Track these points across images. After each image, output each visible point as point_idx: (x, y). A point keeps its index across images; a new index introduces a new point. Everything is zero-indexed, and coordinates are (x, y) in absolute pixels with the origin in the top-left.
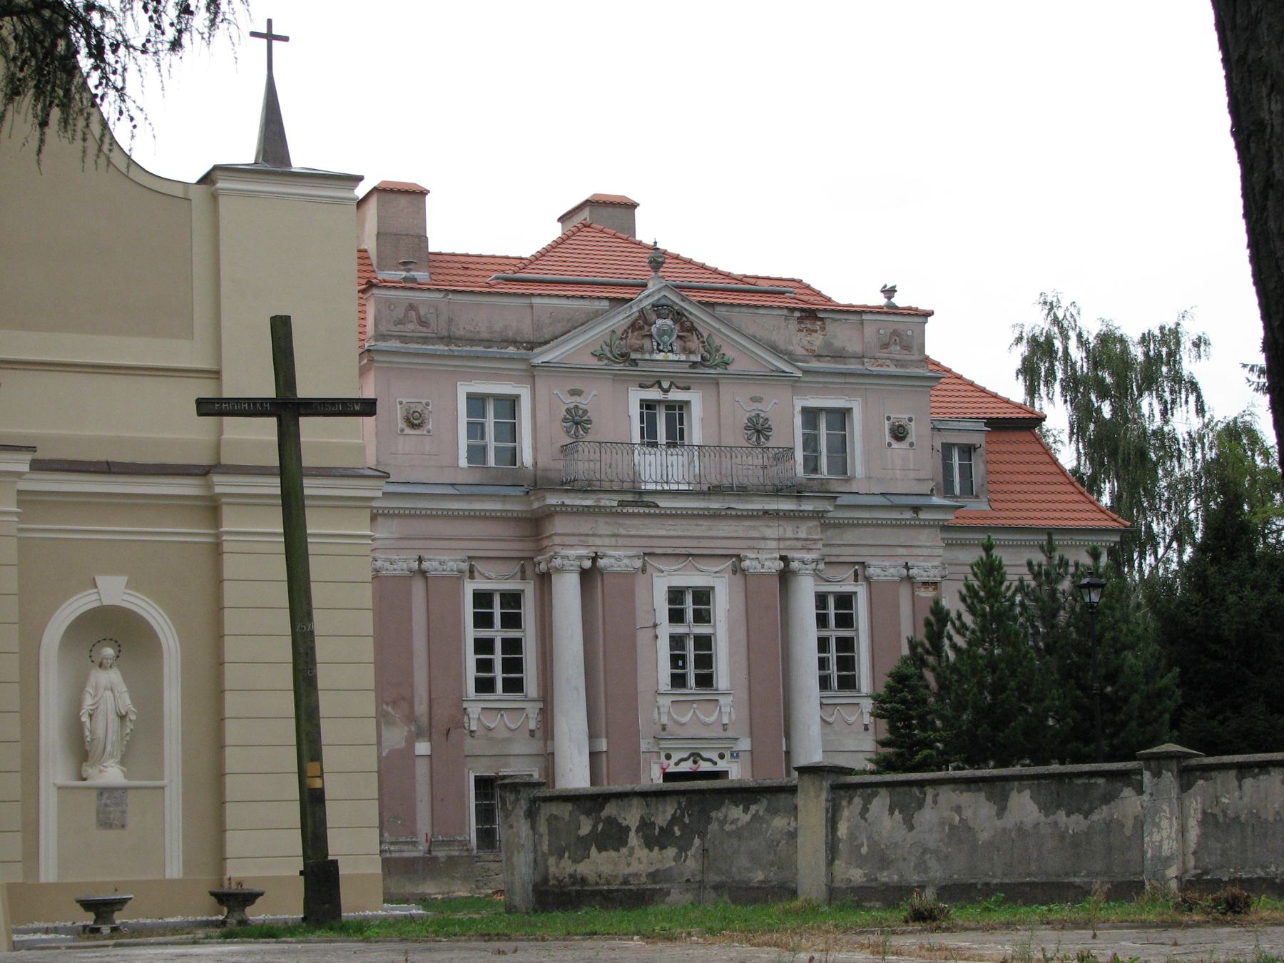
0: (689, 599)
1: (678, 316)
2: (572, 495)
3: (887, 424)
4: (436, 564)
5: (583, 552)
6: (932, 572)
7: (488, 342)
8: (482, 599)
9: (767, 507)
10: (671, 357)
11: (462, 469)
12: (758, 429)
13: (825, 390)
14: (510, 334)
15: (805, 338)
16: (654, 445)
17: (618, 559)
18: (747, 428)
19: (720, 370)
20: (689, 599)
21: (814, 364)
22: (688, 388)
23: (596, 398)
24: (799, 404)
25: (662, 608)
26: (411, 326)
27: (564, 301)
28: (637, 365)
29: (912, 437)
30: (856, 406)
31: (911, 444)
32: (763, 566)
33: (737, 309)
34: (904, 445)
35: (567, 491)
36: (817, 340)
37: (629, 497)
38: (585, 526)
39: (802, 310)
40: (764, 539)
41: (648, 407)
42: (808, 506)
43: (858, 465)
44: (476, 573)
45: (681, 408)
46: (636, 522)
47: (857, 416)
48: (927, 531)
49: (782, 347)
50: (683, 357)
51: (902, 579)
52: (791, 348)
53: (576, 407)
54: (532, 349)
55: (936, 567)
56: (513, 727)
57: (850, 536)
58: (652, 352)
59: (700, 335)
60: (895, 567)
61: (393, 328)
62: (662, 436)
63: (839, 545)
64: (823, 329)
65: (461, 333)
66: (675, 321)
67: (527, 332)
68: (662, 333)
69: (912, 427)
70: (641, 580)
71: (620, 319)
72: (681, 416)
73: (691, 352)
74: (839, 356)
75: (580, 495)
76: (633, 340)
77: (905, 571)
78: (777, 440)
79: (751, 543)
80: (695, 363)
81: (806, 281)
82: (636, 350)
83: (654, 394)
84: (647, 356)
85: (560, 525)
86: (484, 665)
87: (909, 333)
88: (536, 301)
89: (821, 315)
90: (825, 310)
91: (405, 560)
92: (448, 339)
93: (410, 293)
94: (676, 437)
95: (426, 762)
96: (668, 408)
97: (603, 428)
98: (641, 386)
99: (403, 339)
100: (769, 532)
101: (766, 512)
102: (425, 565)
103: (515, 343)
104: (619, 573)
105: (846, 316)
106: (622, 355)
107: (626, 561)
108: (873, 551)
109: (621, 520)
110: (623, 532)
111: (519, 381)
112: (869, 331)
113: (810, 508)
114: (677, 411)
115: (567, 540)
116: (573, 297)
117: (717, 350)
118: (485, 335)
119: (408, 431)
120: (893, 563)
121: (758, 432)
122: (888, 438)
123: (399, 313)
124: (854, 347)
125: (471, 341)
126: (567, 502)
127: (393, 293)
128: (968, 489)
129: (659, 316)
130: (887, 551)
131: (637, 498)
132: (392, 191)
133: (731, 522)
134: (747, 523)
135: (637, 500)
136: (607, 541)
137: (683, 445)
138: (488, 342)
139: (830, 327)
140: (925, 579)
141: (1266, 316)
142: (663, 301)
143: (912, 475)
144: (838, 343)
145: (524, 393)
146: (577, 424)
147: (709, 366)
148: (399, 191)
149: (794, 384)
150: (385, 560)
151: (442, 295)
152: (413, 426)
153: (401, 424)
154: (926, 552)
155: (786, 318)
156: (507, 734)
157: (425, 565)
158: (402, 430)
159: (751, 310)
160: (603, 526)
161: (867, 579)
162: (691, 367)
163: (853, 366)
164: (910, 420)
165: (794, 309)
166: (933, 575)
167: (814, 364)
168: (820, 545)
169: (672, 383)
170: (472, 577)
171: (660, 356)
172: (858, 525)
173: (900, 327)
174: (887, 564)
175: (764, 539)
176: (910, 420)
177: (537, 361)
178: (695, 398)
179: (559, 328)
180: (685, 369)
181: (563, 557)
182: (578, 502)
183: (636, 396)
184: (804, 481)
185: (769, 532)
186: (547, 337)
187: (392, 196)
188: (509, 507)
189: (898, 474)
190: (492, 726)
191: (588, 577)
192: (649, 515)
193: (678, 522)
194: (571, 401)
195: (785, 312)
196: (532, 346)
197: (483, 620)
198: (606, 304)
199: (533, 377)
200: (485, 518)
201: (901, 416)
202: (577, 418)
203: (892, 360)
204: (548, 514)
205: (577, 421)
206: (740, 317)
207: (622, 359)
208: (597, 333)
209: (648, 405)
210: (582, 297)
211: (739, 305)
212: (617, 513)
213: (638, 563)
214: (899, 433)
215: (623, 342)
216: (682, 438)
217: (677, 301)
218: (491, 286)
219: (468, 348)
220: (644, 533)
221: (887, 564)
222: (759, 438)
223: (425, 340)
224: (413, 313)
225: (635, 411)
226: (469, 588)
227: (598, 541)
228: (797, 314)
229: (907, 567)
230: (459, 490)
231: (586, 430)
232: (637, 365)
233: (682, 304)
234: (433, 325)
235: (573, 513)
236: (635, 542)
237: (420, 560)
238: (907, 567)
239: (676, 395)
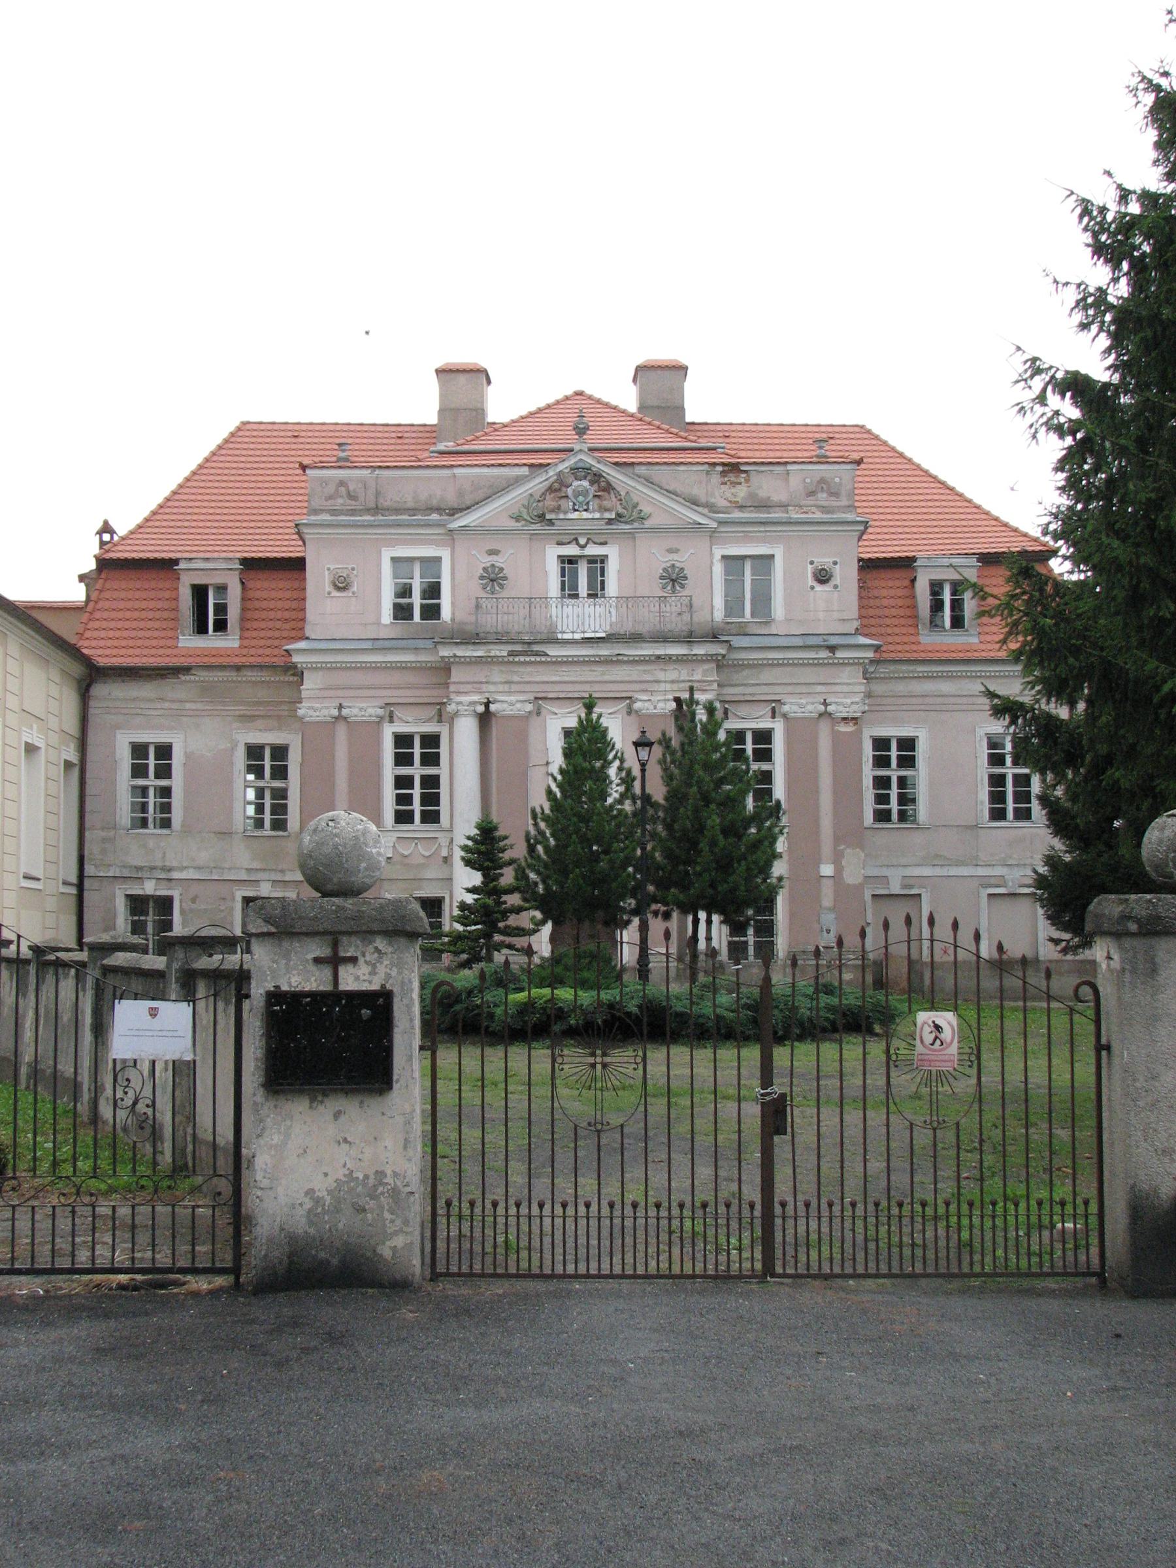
2: (463, 647)
3: (810, 568)
5: (476, 698)
6: (855, 707)
7: (413, 511)
10: (585, 515)
11: (386, 625)
13: (747, 539)
15: (728, 491)
16: (576, 596)
18: (662, 577)
19: (636, 525)
21: (737, 515)
22: (605, 543)
23: (512, 558)
24: (718, 552)
25: (125, 761)
26: (340, 501)
27: (485, 470)
28: (553, 524)
29: (836, 580)
30: (778, 552)
31: (836, 587)
33: (657, 468)
34: (826, 588)
35: (457, 643)
36: (741, 492)
37: (518, 648)
38: (479, 674)
39: (723, 464)
41: (570, 562)
42: (700, 650)
43: (779, 609)
44: (443, 718)
45: (602, 562)
46: (529, 669)
48: (849, 668)
49: (703, 500)
50: (597, 515)
51: (821, 715)
52: (713, 500)
53: (493, 565)
54: (453, 515)
57: (767, 676)
61: (325, 503)
62: (583, 589)
63: (754, 685)
64: (747, 481)
65: (388, 504)
66: (592, 483)
67: (451, 499)
68: (577, 494)
69: (837, 570)
70: (535, 721)
71: (538, 484)
72: (602, 569)
73: (607, 510)
74: (764, 505)
75: (470, 647)
76: (550, 502)
77: (822, 708)
78: (692, 588)
79: (643, 686)
82: (552, 511)
83: (571, 550)
84: (562, 516)
85: (457, 675)
87: (837, 480)
88: (457, 471)
89: (743, 468)
91: (327, 708)
92: (376, 510)
94: (597, 590)
95: (830, 882)
96: (590, 562)
97: (519, 583)
98: (559, 543)
99: (334, 512)
100: (661, 676)
101: (659, 657)
103: (438, 510)
105: (771, 468)
107: (518, 705)
108: (790, 689)
110: (516, 678)
111: (436, 543)
112: (795, 481)
113: (702, 652)
114: (598, 564)
115: (462, 688)
116: (493, 465)
117: (635, 506)
118: (410, 504)
119: (335, 593)
121: (673, 581)
122: (811, 581)
123: (331, 489)
125: (397, 511)
126: (459, 653)
128: (957, 622)
130: (804, 689)
131: (526, 647)
132: (451, 371)
133: (625, 667)
134: (641, 668)
136: (501, 688)
137: (603, 596)
138: (413, 511)
139: (754, 478)
140: (845, 715)
142: (581, 465)
143: (836, 615)
144: (762, 494)
147: (626, 520)
148: (458, 371)
149: (713, 536)
150: (309, 708)
151: (369, 471)
152: (339, 589)
153: (328, 587)
154: (845, 689)
155: (708, 473)
156: (422, 861)
157: (345, 712)
159: (672, 467)
160: (497, 675)
161: (784, 716)
162: (608, 524)
164: (835, 563)
165: (714, 464)
167: (737, 515)
169: (589, 539)
170: (391, 721)
171: (575, 515)
173: (827, 475)
174: (803, 701)
176: (835, 563)
177: (454, 525)
178: (612, 552)
179: (480, 495)
180: (602, 525)
181: (458, 703)
183: (552, 554)
184: (722, 625)
185: (661, 676)
186: (468, 503)
187: (453, 375)
189: (821, 615)
190: (406, 853)
191: (485, 719)
192: (541, 662)
194: (488, 560)
195: (706, 467)
196: (454, 512)
197: (403, 759)
199: (453, 539)
202: (493, 576)
203: (817, 507)
204: (445, 668)
205: (493, 578)
206: (662, 475)
207: (540, 518)
208: (517, 495)
209: (568, 562)
210: (500, 465)
214: (823, 577)
216: (603, 589)
217: (594, 463)
220: (538, 679)
222: (673, 586)
223: (353, 512)
224: (343, 489)
225: (553, 568)
227: (492, 688)
229: (825, 703)
230: (378, 644)
231: (502, 586)
232: (553, 524)
233: (598, 466)
234: (362, 499)
235: (470, 663)
236: (527, 688)
237: (341, 707)
238: (825, 703)
239: (593, 550)
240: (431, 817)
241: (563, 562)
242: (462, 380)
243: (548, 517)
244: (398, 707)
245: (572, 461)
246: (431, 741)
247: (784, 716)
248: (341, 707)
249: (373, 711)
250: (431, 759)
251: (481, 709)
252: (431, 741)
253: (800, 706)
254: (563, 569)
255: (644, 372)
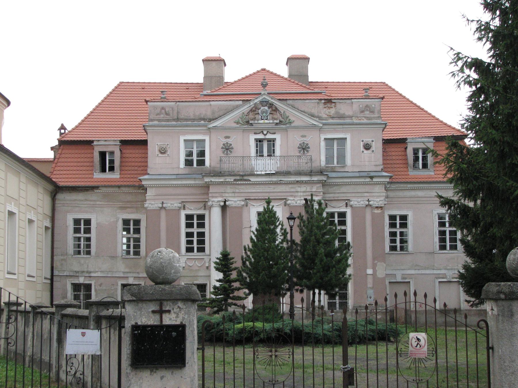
0: (132, 223)
1: (271, 105)
2: (214, 178)
3: (362, 144)
4: (169, 205)
5: (220, 199)
6: (381, 202)
7: (193, 120)
8: (189, 217)
9: (297, 179)
10: (266, 121)
11: (181, 168)
12: (304, 148)
13: (335, 131)
14: (202, 116)
15: (327, 111)
16: (262, 156)
17: (235, 202)
18: (299, 148)
19: (288, 125)
20: (132, 223)
21: (331, 121)
22: (275, 133)
24: (323, 137)
26: (162, 116)
28: (253, 125)
29: (373, 148)
30: (348, 136)
31: (373, 151)
32: (296, 203)
34: (369, 152)
35: (212, 176)
36: (332, 111)
37: (238, 178)
38: (221, 189)
39: (325, 100)
40: (297, 192)
41: (260, 141)
43: (349, 161)
45: (274, 141)
46: (243, 187)
47: (348, 142)
49: (316, 115)
50: (271, 121)
52: (320, 115)
53: (227, 143)
54: (210, 121)
55: (382, 200)
56: (199, 265)
57: (344, 189)
58: (258, 120)
59: (280, 112)
60: (363, 201)
62: (265, 153)
63: (338, 193)
64: (335, 106)
65: (182, 117)
66: (269, 108)
67: (209, 115)
68: (263, 112)
70: (245, 209)
71: (246, 108)
72: (274, 144)
73: (275, 119)
74: (342, 117)
76: (251, 116)
77: (367, 203)
79: (291, 194)
80: (277, 123)
81: (387, 83)
82: (252, 120)
83: (261, 136)
84: (256, 122)
85: (212, 189)
86: (190, 242)
89: (333, 101)
90: (335, 99)
92: (178, 119)
93: (163, 103)
96: (268, 141)
97: (238, 150)
98: (255, 133)
99: (159, 120)
100: (299, 189)
101: (298, 181)
102: (164, 205)
103: (204, 119)
104: (235, 207)
106: (246, 122)
107: (238, 202)
108: (353, 195)
109: (237, 187)
110: (237, 191)
111: (204, 134)
115: (214, 195)
118: (192, 117)
119: (160, 155)
120: (363, 199)
121: (303, 149)
122: (362, 149)
123: (158, 111)
124: (349, 113)
125: (186, 120)
126: (213, 180)
127: (156, 103)
128: (425, 166)
129: (263, 106)
130: (360, 195)
131: (241, 178)
132: (209, 60)
134: (290, 186)
135: (243, 177)
136: (230, 195)
138: (193, 120)
139: (338, 105)
140: (377, 206)
141: (3, 115)
142: (264, 100)
144: (342, 112)
145: (207, 138)
146: (227, 149)
147: (284, 123)
148: (212, 60)
150: (150, 204)
151: (174, 103)
152: (162, 153)
153: (157, 152)
156: (197, 268)
157: (164, 205)
158: (158, 155)
159: (303, 101)
160: (229, 189)
161: (351, 206)
163: (348, 121)
164: (373, 141)
166: (381, 204)
167: (331, 121)
168: (322, 194)
170: (184, 209)
171: (262, 121)
172: (346, 185)
174: (359, 200)
175: (297, 192)
176: (373, 141)
178: (278, 137)
179: (221, 113)
181: (212, 201)
182: (217, 180)
183: (252, 138)
185: (299, 189)
186: (217, 116)
188: (197, 182)
189: (367, 163)
191: (224, 208)
193: (262, 186)
194: (225, 141)
195: (317, 101)
196: (210, 120)
197: (189, 225)
198: (241, 102)
200: (189, 187)
201: (368, 140)
202: (227, 147)
204: (207, 186)
205: (227, 148)
207: (247, 123)
208: (237, 113)
209: (259, 141)
210: (230, 100)
211: (297, 99)
212: (234, 184)
213: (243, 203)
214: (367, 147)
215: (247, 117)
216: (274, 152)
217: (270, 99)
218: (196, 98)
219: (185, 123)
221: (359, 200)
222: (304, 151)
223: (168, 121)
224: (163, 111)
225: (253, 144)
226: (183, 214)
227: (227, 195)
228: (323, 101)
229: (368, 201)
230: (179, 177)
232: (253, 125)
233: (272, 100)
234: (171, 115)
236: (242, 195)
237: (163, 203)
238: (368, 201)
239: (269, 136)
240: (201, 250)
241: (257, 141)
242: (214, 64)
243: (250, 122)
244: (188, 204)
245: (260, 98)
246: (201, 217)
247: (351, 206)
248: (163, 203)
249: (176, 205)
250: (201, 225)
251: (222, 204)
252: (201, 217)
253: (357, 202)
254: (257, 145)
255: (290, 60)
